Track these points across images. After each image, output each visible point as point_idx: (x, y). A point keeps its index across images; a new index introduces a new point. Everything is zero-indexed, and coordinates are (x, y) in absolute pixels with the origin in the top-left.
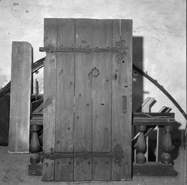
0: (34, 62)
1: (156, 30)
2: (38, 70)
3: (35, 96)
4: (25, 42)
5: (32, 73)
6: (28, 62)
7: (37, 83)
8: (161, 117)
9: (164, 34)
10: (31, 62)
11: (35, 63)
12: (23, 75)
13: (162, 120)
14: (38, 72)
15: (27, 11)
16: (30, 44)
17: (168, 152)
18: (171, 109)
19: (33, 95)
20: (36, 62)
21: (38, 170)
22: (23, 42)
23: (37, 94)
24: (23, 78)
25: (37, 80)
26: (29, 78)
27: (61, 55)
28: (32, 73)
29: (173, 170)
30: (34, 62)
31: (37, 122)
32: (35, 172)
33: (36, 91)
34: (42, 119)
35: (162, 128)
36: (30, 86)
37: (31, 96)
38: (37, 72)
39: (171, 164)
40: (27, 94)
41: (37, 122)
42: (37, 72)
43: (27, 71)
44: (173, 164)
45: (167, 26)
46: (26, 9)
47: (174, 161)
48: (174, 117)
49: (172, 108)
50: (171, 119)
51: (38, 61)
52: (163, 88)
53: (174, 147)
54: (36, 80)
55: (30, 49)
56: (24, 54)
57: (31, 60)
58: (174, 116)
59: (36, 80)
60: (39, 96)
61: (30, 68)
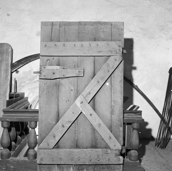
0: (13, 62)
1: (131, 32)
2: (18, 70)
3: (13, 94)
4: (5, 43)
5: (12, 73)
6: (7, 62)
7: (16, 82)
8: (128, 115)
9: (139, 36)
10: (10, 62)
11: (14, 63)
12: (2, 75)
13: (129, 118)
14: (18, 71)
15: (8, 15)
16: (10, 45)
17: (136, 150)
18: (138, 107)
19: (11, 93)
20: (15, 63)
21: (8, 165)
22: (4, 44)
23: (16, 93)
24: (2, 77)
25: (16, 80)
26: (7, 77)
27: (113, 81)
28: (12, 73)
29: (141, 167)
30: (13, 62)
31: (7, 118)
32: (5, 167)
33: (15, 90)
34: (38, 116)
35: (130, 125)
36: (9, 85)
37: (10, 94)
38: (17, 71)
39: (138, 161)
40: (6, 92)
41: (7, 118)
42: (17, 71)
43: (7, 71)
44: (140, 161)
45: (141, 29)
46: (8, 13)
47: (85, 170)
48: (141, 114)
49: (139, 106)
50: (139, 116)
51: (17, 62)
52: (138, 88)
53: (141, 145)
54: (15, 80)
55: (10, 50)
56: (4, 54)
57: (10, 60)
58: (141, 114)
59: (15, 80)
60: (17, 94)
61: (9, 67)
